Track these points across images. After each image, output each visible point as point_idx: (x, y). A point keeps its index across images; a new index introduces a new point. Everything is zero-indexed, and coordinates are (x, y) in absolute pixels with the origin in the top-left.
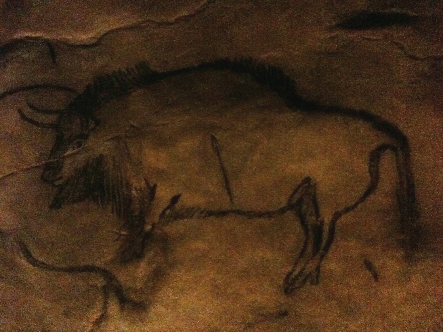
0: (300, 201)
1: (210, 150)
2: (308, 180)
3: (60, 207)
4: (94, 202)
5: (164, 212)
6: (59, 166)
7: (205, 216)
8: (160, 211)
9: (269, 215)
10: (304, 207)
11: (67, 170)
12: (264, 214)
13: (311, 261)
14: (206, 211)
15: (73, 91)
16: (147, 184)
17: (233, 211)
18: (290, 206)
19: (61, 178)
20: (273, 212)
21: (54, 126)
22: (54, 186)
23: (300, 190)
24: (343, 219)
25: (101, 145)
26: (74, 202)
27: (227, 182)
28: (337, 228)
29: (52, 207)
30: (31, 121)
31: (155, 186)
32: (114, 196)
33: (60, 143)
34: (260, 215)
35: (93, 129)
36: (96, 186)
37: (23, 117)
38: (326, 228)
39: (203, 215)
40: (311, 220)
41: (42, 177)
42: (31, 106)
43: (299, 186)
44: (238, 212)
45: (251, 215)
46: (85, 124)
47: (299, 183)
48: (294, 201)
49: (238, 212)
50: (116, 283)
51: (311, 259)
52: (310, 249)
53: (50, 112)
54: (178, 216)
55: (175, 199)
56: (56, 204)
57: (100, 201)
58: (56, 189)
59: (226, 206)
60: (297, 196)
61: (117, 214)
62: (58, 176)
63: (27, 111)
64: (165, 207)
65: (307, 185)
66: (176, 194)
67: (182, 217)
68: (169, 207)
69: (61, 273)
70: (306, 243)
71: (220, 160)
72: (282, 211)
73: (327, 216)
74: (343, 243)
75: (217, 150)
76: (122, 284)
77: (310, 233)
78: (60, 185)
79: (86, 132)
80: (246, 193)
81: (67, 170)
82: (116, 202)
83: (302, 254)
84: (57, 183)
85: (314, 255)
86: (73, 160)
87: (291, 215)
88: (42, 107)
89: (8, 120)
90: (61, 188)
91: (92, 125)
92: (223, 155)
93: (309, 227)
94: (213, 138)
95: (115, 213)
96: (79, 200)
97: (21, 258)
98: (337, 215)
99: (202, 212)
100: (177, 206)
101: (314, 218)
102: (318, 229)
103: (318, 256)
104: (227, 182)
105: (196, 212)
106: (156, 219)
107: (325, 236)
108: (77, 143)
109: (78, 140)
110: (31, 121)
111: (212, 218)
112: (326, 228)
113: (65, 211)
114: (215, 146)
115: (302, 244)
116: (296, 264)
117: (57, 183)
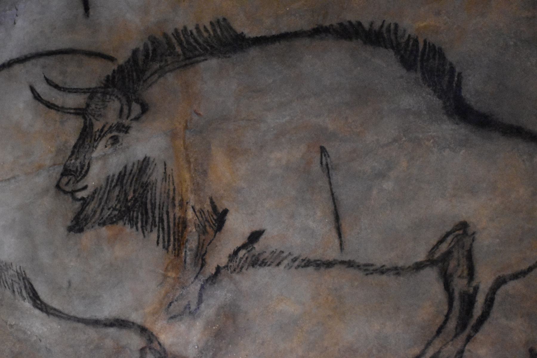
0: (449, 253)
1: (316, 167)
2: (464, 226)
3: (81, 230)
4: (132, 227)
5: (236, 253)
6: (82, 172)
7: (298, 266)
8: (230, 248)
9: (397, 271)
10: (452, 264)
11: (95, 177)
12: (388, 270)
13: (451, 343)
14: (301, 258)
15: (111, 59)
16: (214, 208)
17: (343, 263)
18: (430, 262)
19: (85, 188)
20: (402, 269)
21: (80, 112)
22: (75, 199)
23: (449, 239)
24: (511, 287)
25: (147, 143)
26: (103, 224)
27: (337, 218)
28: (498, 298)
29: (70, 229)
30: (50, 105)
31: (226, 212)
32: (161, 220)
33: (87, 137)
34: (382, 271)
35: (137, 119)
36: (134, 202)
37: (37, 97)
38: (480, 300)
39: (296, 263)
40: (459, 285)
41: (58, 186)
42: (48, 81)
43: (448, 234)
44: (350, 264)
45: (368, 269)
46: (126, 111)
47: (448, 229)
48: (437, 255)
49: (350, 264)
50: (158, 348)
51: (452, 340)
52: (452, 324)
53: (76, 91)
54: (257, 262)
55: (255, 236)
56: (77, 226)
57: (139, 225)
58: (78, 205)
59: (332, 254)
60: (444, 247)
61: (164, 247)
62: (80, 185)
63: (42, 88)
64: (239, 244)
65: (461, 232)
66: (256, 228)
67: (264, 264)
68: (244, 246)
69: (80, 325)
70: (447, 317)
71: (330, 184)
72: (418, 267)
73: (485, 279)
74: (503, 321)
75: (327, 169)
76: (167, 347)
77: (456, 304)
78: (83, 199)
79: (126, 122)
80: (367, 242)
81: (95, 177)
82: (163, 229)
83: (439, 332)
84: (79, 195)
85: (456, 335)
86: (104, 164)
87: (431, 275)
88: (65, 83)
89: (19, 106)
90: (85, 202)
91: (136, 109)
92: (337, 178)
93: (456, 295)
94: (323, 150)
95: (161, 245)
96: (111, 221)
97: (24, 299)
98: (500, 282)
99: (294, 260)
100: (258, 247)
101: (465, 281)
102: (469, 301)
103: (463, 336)
104: (337, 218)
105: (286, 258)
106: (223, 261)
107: (478, 311)
108: (112, 137)
109: (113, 134)
110: (50, 105)
111: (310, 269)
112: (480, 300)
113: (88, 237)
114: (324, 163)
115: (442, 318)
116: (429, 344)
117: (79, 195)
